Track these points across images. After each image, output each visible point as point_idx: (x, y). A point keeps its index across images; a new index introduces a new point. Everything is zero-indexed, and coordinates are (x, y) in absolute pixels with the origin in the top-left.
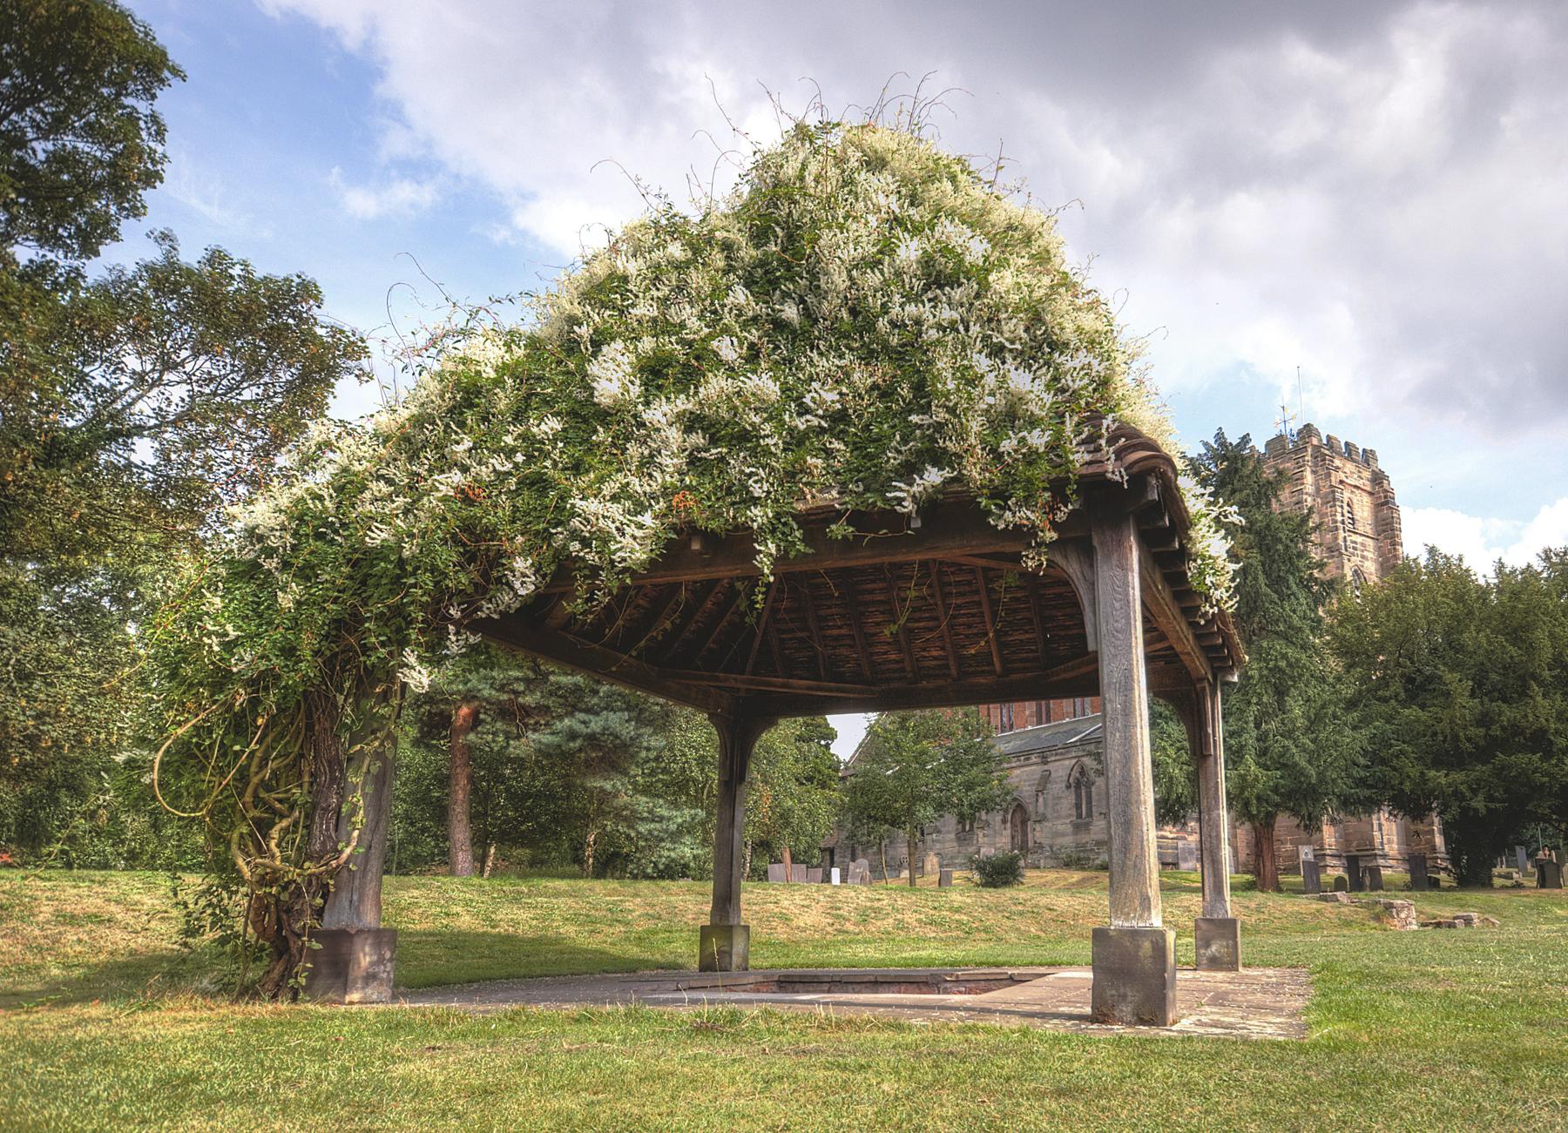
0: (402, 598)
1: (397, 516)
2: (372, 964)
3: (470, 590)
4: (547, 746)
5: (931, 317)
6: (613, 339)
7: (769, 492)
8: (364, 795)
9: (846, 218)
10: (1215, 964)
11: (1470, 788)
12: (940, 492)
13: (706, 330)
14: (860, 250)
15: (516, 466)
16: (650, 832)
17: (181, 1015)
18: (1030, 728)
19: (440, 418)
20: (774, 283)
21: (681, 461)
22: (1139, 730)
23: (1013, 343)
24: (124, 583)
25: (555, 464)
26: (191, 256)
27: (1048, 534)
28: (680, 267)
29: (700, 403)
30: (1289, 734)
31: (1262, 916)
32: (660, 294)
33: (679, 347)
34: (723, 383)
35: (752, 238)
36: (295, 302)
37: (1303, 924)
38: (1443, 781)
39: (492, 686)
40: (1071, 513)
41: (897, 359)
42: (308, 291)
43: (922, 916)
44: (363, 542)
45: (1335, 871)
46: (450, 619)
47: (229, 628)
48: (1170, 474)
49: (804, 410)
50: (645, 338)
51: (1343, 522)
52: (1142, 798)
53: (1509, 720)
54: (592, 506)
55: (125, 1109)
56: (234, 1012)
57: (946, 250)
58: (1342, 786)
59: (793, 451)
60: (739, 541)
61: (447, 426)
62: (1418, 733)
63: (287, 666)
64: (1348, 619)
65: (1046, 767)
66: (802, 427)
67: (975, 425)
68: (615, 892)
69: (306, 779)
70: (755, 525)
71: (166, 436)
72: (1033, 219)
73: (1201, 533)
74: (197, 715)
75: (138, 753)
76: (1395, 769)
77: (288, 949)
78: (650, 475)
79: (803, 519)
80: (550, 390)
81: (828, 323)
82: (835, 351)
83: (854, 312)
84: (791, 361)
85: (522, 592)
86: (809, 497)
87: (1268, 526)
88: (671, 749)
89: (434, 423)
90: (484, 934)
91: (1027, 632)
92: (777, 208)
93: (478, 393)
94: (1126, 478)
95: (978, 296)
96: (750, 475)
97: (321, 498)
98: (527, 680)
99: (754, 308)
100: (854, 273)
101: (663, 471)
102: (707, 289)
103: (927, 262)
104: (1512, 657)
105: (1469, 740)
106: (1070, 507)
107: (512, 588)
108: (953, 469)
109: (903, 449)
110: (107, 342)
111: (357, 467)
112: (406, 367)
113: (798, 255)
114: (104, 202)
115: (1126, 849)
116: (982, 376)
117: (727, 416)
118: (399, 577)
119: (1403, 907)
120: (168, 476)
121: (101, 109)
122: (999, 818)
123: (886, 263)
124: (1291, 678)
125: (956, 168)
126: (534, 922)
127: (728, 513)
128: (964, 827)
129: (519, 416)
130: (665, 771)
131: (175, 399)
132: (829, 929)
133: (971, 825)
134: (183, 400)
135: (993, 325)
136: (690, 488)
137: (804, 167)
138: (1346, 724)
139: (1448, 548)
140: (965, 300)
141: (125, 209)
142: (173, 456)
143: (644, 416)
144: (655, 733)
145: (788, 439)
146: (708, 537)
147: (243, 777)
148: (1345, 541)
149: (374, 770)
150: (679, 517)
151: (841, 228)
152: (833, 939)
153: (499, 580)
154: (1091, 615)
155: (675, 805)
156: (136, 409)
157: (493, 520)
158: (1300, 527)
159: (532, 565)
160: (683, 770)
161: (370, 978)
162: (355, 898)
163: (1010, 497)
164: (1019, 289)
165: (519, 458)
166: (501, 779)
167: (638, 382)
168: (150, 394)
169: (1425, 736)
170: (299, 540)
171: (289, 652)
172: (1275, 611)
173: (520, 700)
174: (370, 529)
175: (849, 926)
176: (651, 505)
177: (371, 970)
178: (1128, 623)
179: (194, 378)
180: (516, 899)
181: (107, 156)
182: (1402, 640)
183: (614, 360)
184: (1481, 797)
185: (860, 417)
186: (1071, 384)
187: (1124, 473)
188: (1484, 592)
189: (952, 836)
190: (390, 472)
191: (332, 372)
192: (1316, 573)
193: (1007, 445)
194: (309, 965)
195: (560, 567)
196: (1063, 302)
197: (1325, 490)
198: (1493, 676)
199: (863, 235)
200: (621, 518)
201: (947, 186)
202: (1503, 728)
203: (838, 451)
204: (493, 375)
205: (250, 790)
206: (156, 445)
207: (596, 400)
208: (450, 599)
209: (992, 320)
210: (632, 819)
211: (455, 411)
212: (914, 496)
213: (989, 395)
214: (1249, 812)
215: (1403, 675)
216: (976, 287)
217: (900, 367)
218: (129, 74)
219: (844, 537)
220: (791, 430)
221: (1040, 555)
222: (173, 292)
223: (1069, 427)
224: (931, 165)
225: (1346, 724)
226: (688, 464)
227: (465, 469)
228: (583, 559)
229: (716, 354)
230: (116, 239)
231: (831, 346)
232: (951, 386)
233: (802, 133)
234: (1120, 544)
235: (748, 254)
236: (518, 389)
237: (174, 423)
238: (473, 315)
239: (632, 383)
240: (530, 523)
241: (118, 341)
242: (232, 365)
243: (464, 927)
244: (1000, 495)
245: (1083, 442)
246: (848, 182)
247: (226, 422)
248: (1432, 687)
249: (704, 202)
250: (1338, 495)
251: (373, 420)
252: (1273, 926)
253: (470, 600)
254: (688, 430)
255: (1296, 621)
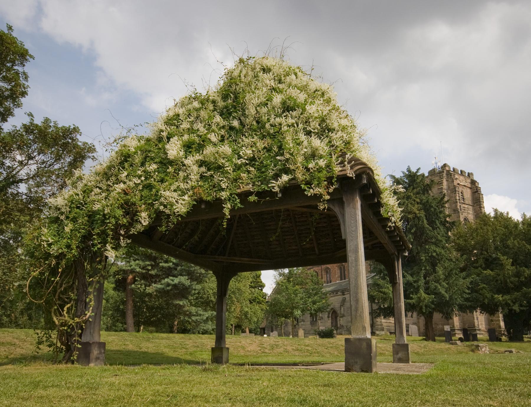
0: (105, 228)
1: (103, 200)
2: (98, 354)
3: (127, 224)
4: (159, 289)
5: (285, 122)
6: (174, 136)
7: (228, 186)
8: (94, 296)
9: (255, 89)
10: (400, 360)
11: (512, 301)
12: (288, 184)
13: (206, 131)
14: (260, 100)
15: (142, 181)
16: (197, 320)
17: (37, 368)
18: (338, 282)
19: (117, 166)
20: (230, 114)
21: (198, 177)
22: (361, 267)
23: (314, 130)
24: (17, 235)
25: (155, 179)
26: (38, 121)
27: (326, 196)
28: (197, 110)
29: (204, 157)
30: (437, 281)
31: (426, 349)
32: (191, 120)
33: (197, 138)
34: (212, 149)
35: (222, 98)
36: (71, 134)
37: (442, 352)
38: (501, 299)
39: (140, 267)
40: (335, 189)
41: (273, 138)
42: (76, 130)
43: (294, 348)
44: (92, 208)
45: (459, 335)
46: (121, 235)
47: (50, 239)
48: (371, 173)
49: (240, 157)
50: (185, 135)
51: (459, 200)
52: (362, 291)
53: (528, 275)
54: (167, 193)
55: (20, 388)
56: (53, 367)
57: (290, 98)
58: (459, 301)
59: (236, 171)
60: (218, 203)
61: (119, 169)
62: (490, 280)
63: (68, 251)
64: (461, 237)
65: (344, 296)
66: (240, 163)
67: (300, 159)
68: (183, 338)
69: (75, 290)
70: (223, 198)
71: (30, 182)
72: (324, 87)
73: (385, 196)
74: (40, 269)
75: (21, 283)
76: (480, 294)
77: (70, 349)
78: (187, 183)
79: (239, 195)
80: (153, 155)
81: (249, 127)
82: (251, 136)
83: (258, 122)
84: (236, 141)
85: (144, 224)
86: (241, 187)
87: (427, 201)
88: (203, 290)
89: (115, 168)
90: (137, 351)
91: (327, 239)
92: (231, 87)
93: (129, 157)
94: (354, 175)
95: (302, 114)
96: (221, 181)
97: (78, 195)
98: (151, 265)
99: (222, 123)
100: (258, 108)
101: (191, 181)
102: (207, 117)
103: (284, 103)
104: (528, 249)
105: (511, 282)
106: (334, 187)
107: (141, 223)
108: (292, 175)
109: (274, 169)
110: (9, 151)
111: (89, 184)
112: (107, 150)
113: (238, 103)
114: (9, 103)
115: (357, 310)
116: (303, 142)
117: (213, 161)
118: (104, 220)
119: (483, 347)
120: (31, 197)
121: (7, 71)
122: (326, 316)
123: (269, 104)
124: (438, 260)
125: (297, 71)
126: (154, 348)
127: (214, 194)
128: (313, 319)
129: (143, 164)
130: (201, 298)
131: (33, 170)
132: (260, 352)
133: (316, 318)
134: (35, 170)
135: (307, 124)
136: (200, 186)
137: (241, 72)
138: (460, 277)
139: (502, 210)
140: (297, 115)
141: (16, 105)
142: (32, 190)
143: (185, 162)
144: (197, 284)
145: (234, 167)
146: (207, 203)
147: (55, 291)
148: (460, 206)
149: (97, 287)
150: (197, 196)
151: (253, 93)
152: (261, 355)
153: (136, 220)
154: (343, 226)
155: (205, 310)
156: (20, 174)
157: (134, 200)
158: (441, 202)
159: (148, 215)
160: (208, 297)
161: (97, 359)
162: (92, 331)
163: (312, 184)
164: (318, 112)
165: (143, 178)
166: (144, 302)
167: (183, 150)
168: (25, 168)
169: (493, 281)
170: (71, 209)
171: (68, 246)
172: (431, 234)
173: (150, 272)
174: (94, 204)
175: (267, 351)
176: (187, 193)
177: (97, 356)
178: (357, 228)
179: (38, 162)
180: (148, 340)
181: (9, 87)
182: (483, 245)
183: (174, 143)
184: (517, 305)
185: (259, 159)
186: (335, 143)
187: (353, 174)
188: (516, 225)
189: (309, 323)
190: (100, 185)
191: (83, 157)
192: (448, 219)
193: (310, 166)
194: (77, 353)
195: (157, 215)
196: (334, 115)
197: (451, 187)
198: (521, 257)
199: (261, 95)
200: (177, 197)
201: (293, 77)
202: (526, 278)
203: (252, 171)
204: (134, 150)
205: (57, 294)
206: (27, 186)
207: (168, 157)
208: (121, 228)
209: (307, 122)
210: (190, 315)
211: (121, 163)
212: (278, 185)
213: (305, 148)
214: (422, 311)
215: (484, 258)
216: (301, 110)
217: (274, 140)
218: (16, 58)
219: (254, 201)
220: (235, 165)
221: (324, 204)
222: (31, 133)
223: (334, 157)
224: (288, 70)
225: (460, 277)
226: (200, 178)
227: (125, 183)
228: (164, 212)
229: (210, 139)
230: (13, 116)
231: (250, 135)
232: (291, 145)
233: (241, 61)
234: (353, 199)
235: (221, 104)
236: (142, 155)
237: (32, 178)
238: (129, 131)
239: (181, 151)
240: (147, 200)
241: (14, 150)
242: (51, 157)
243: (130, 349)
244: (309, 183)
245: (340, 164)
246: (256, 76)
247: (49, 177)
248: (496, 262)
249: (207, 88)
250: (457, 189)
251: (95, 168)
252: (430, 353)
253: (128, 227)
254: (200, 166)
255: (439, 237)
